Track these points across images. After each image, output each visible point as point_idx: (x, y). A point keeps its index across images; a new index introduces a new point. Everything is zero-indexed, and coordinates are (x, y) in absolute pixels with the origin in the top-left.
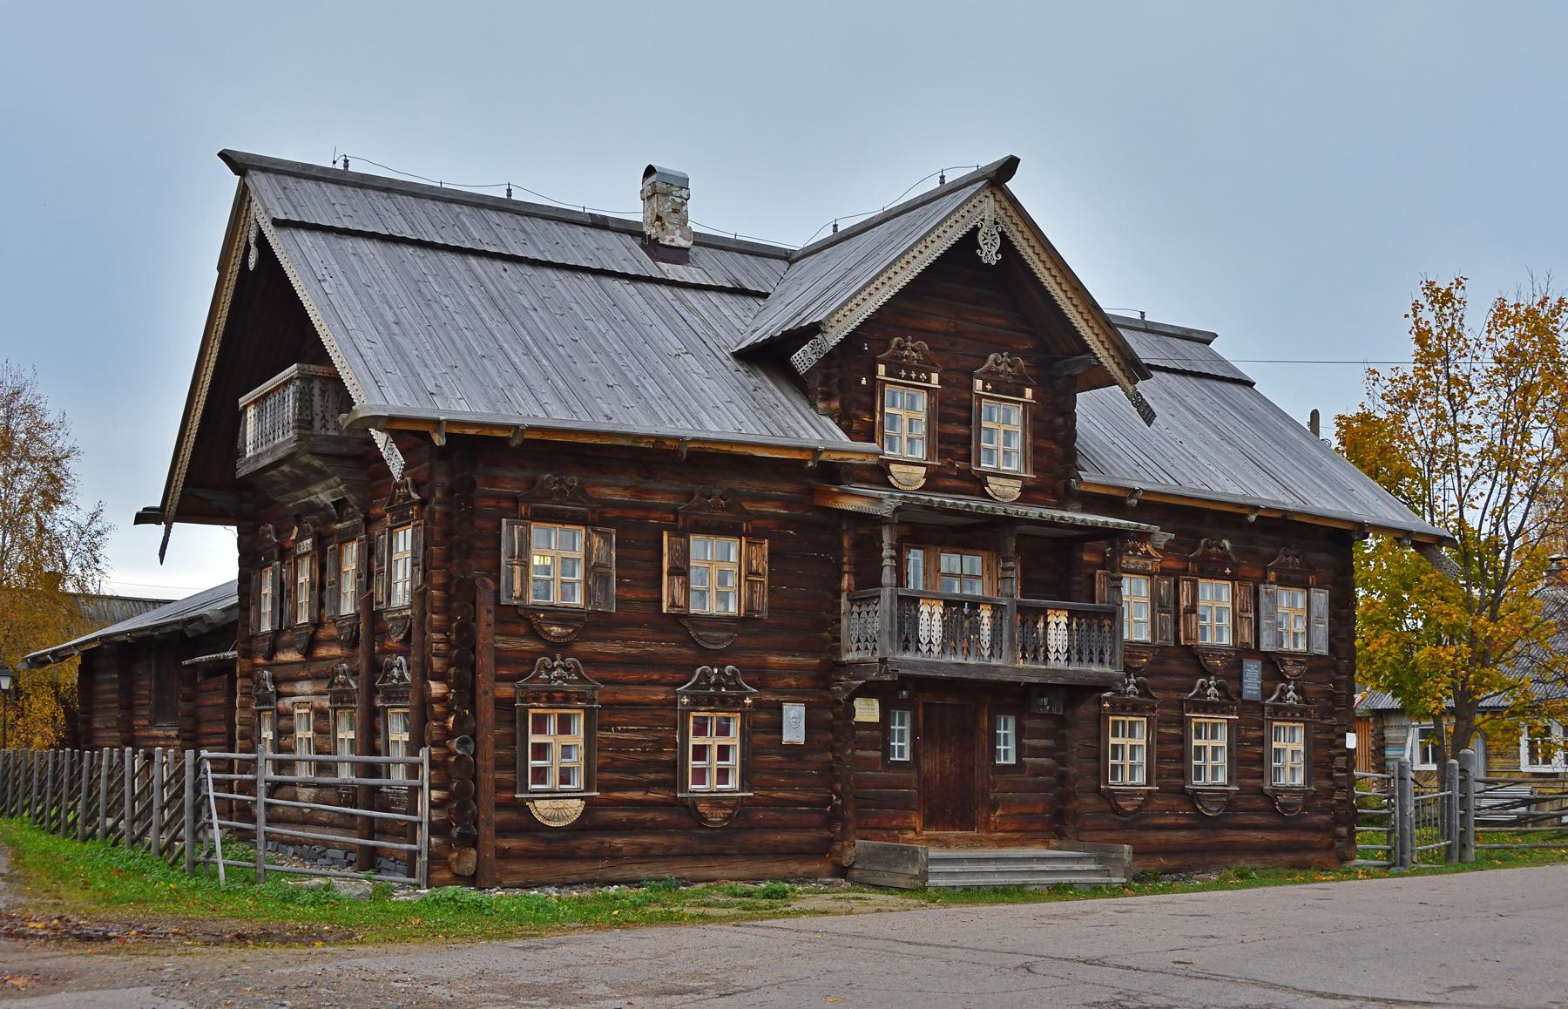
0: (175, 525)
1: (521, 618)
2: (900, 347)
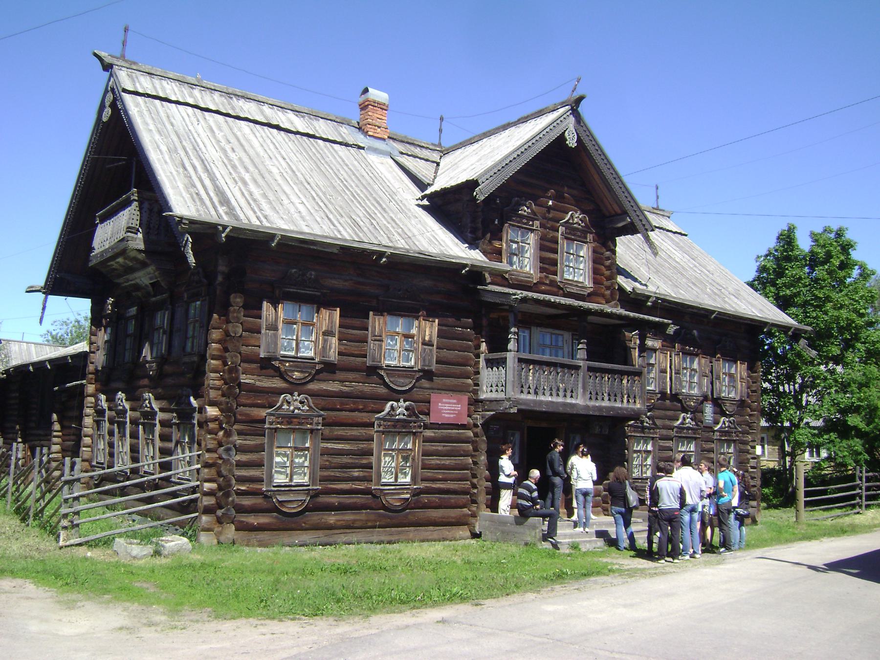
0: (50, 297)
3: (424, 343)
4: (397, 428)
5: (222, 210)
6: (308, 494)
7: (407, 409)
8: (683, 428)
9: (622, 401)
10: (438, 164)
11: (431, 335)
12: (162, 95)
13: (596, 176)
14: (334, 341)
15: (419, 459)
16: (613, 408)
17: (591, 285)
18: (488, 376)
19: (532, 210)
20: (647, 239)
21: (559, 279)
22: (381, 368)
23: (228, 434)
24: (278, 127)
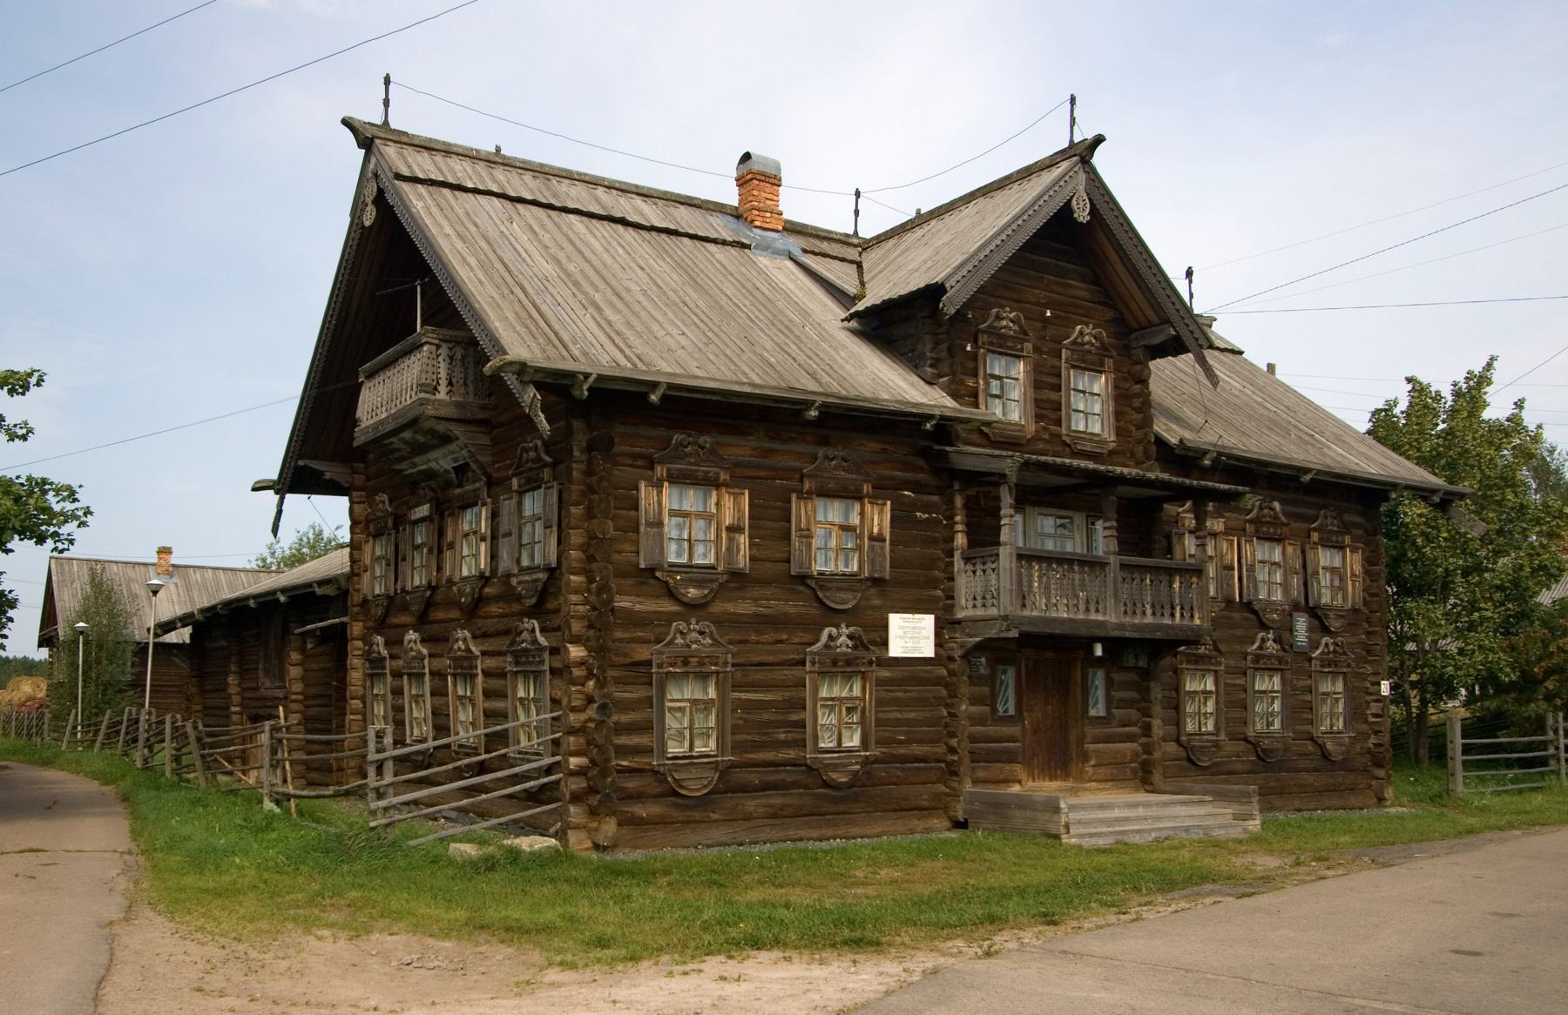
0: (288, 496)
1: (650, 577)
2: (998, 318)
3: (872, 538)
4: (840, 667)
5: (551, 351)
6: (716, 769)
7: (850, 637)
8: (1264, 656)
9: (1173, 615)
10: (859, 266)
11: (880, 529)
12: (451, 180)
13: (1120, 268)
14: (743, 540)
15: (871, 716)
16: (1160, 627)
17: (1113, 438)
18: (966, 583)
19: (1021, 327)
20: (1202, 361)
21: (1064, 431)
22: (812, 577)
23: (601, 684)
24: (623, 222)
